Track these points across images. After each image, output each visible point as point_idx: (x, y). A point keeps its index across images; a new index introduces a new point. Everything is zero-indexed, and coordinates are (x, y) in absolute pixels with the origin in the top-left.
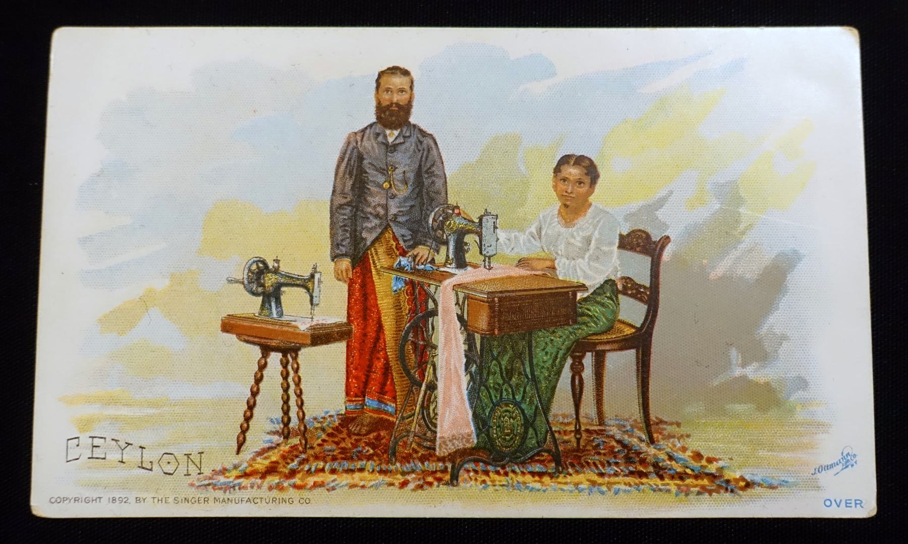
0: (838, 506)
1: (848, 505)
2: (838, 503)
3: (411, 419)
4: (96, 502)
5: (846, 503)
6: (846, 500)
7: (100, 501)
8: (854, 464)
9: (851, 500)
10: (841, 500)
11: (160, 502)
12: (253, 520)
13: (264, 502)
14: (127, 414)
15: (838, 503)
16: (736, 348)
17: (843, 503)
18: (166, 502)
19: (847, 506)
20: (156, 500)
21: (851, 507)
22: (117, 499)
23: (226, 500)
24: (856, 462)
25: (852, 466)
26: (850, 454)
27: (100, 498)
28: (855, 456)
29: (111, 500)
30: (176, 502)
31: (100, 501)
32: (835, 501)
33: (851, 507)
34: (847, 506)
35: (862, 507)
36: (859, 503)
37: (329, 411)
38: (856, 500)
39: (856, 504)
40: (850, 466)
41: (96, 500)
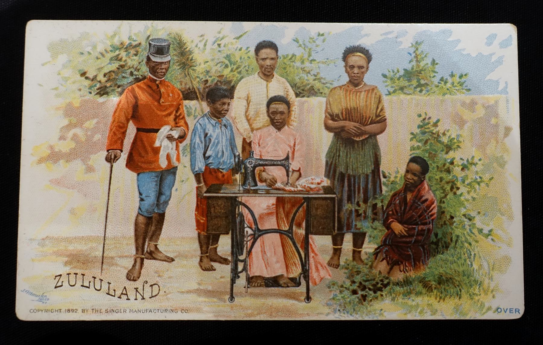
0: (505, 312)
1: (511, 312)
2: (505, 311)
3: (290, 218)
4: (58, 312)
5: (510, 311)
6: (510, 309)
7: (60, 312)
8: (45, 303)
9: (513, 309)
10: (507, 309)
11: (97, 312)
12: (72, 322)
13: (160, 311)
14: (453, 96)
15: (505, 311)
16: (74, 149)
17: (508, 310)
18: (100, 312)
19: (510, 313)
20: (94, 311)
21: (513, 313)
22: (70, 311)
23: (137, 311)
24: (46, 303)
25: (43, 303)
26: (47, 297)
27: (60, 310)
28: (48, 299)
29: (67, 311)
30: (106, 312)
31: (60, 312)
32: (504, 309)
33: (513, 313)
34: (510, 313)
35: (519, 313)
36: (517, 311)
37: (468, 159)
38: (516, 309)
39: (516, 311)
40: (42, 302)
41: (58, 311)
